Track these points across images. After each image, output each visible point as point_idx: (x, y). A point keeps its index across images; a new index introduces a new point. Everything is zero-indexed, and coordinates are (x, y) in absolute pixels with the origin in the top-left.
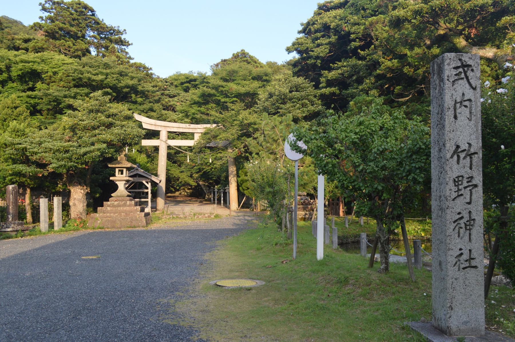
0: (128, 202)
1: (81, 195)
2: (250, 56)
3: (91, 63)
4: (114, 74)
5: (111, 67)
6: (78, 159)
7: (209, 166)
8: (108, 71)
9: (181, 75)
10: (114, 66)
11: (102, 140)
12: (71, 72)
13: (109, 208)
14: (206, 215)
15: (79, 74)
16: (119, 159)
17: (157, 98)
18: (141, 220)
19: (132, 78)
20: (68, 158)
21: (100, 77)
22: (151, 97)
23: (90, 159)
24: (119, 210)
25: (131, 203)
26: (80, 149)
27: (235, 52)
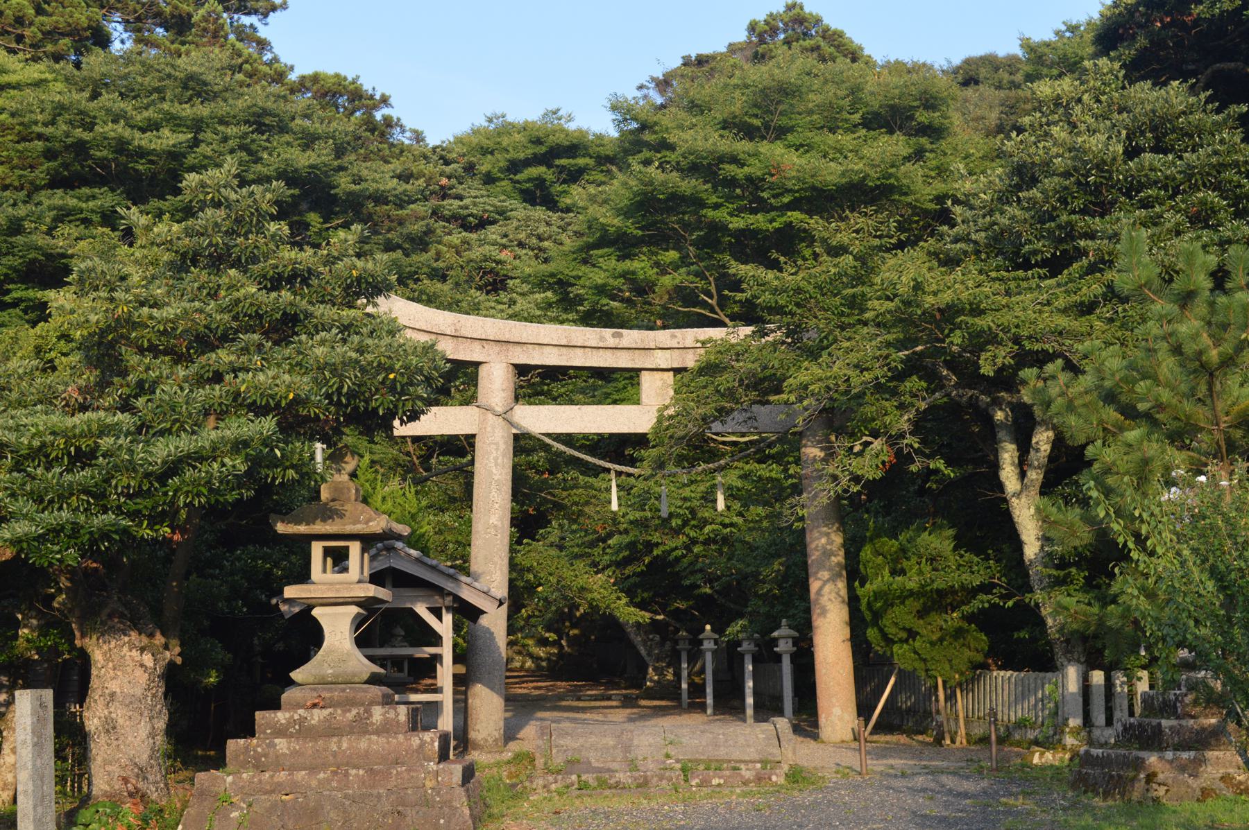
0: (378, 713)
1: (142, 677)
2: (827, 30)
3: (125, 77)
4: (227, 124)
5: (216, 95)
6: (139, 493)
7: (677, 532)
8: (203, 110)
9: (507, 129)
10: (226, 90)
11: (253, 397)
12: (40, 117)
13: (282, 744)
14: (747, 774)
15: (74, 127)
16: (325, 495)
17: (416, 228)
18: (447, 803)
19: (309, 140)
20: (86, 492)
21: (168, 139)
22: (387, 223)
23: (198, 495)
24: (335, 754)
25: (392, 715)
26: (147, 443)
27: (761, 17)
